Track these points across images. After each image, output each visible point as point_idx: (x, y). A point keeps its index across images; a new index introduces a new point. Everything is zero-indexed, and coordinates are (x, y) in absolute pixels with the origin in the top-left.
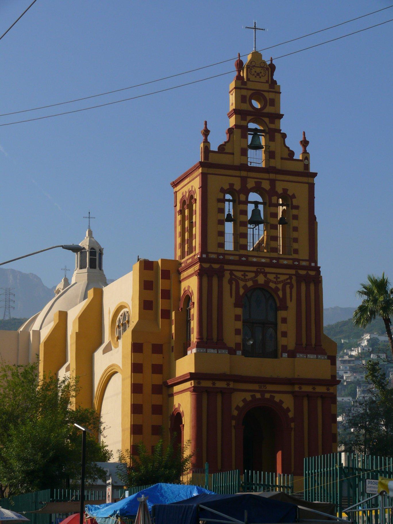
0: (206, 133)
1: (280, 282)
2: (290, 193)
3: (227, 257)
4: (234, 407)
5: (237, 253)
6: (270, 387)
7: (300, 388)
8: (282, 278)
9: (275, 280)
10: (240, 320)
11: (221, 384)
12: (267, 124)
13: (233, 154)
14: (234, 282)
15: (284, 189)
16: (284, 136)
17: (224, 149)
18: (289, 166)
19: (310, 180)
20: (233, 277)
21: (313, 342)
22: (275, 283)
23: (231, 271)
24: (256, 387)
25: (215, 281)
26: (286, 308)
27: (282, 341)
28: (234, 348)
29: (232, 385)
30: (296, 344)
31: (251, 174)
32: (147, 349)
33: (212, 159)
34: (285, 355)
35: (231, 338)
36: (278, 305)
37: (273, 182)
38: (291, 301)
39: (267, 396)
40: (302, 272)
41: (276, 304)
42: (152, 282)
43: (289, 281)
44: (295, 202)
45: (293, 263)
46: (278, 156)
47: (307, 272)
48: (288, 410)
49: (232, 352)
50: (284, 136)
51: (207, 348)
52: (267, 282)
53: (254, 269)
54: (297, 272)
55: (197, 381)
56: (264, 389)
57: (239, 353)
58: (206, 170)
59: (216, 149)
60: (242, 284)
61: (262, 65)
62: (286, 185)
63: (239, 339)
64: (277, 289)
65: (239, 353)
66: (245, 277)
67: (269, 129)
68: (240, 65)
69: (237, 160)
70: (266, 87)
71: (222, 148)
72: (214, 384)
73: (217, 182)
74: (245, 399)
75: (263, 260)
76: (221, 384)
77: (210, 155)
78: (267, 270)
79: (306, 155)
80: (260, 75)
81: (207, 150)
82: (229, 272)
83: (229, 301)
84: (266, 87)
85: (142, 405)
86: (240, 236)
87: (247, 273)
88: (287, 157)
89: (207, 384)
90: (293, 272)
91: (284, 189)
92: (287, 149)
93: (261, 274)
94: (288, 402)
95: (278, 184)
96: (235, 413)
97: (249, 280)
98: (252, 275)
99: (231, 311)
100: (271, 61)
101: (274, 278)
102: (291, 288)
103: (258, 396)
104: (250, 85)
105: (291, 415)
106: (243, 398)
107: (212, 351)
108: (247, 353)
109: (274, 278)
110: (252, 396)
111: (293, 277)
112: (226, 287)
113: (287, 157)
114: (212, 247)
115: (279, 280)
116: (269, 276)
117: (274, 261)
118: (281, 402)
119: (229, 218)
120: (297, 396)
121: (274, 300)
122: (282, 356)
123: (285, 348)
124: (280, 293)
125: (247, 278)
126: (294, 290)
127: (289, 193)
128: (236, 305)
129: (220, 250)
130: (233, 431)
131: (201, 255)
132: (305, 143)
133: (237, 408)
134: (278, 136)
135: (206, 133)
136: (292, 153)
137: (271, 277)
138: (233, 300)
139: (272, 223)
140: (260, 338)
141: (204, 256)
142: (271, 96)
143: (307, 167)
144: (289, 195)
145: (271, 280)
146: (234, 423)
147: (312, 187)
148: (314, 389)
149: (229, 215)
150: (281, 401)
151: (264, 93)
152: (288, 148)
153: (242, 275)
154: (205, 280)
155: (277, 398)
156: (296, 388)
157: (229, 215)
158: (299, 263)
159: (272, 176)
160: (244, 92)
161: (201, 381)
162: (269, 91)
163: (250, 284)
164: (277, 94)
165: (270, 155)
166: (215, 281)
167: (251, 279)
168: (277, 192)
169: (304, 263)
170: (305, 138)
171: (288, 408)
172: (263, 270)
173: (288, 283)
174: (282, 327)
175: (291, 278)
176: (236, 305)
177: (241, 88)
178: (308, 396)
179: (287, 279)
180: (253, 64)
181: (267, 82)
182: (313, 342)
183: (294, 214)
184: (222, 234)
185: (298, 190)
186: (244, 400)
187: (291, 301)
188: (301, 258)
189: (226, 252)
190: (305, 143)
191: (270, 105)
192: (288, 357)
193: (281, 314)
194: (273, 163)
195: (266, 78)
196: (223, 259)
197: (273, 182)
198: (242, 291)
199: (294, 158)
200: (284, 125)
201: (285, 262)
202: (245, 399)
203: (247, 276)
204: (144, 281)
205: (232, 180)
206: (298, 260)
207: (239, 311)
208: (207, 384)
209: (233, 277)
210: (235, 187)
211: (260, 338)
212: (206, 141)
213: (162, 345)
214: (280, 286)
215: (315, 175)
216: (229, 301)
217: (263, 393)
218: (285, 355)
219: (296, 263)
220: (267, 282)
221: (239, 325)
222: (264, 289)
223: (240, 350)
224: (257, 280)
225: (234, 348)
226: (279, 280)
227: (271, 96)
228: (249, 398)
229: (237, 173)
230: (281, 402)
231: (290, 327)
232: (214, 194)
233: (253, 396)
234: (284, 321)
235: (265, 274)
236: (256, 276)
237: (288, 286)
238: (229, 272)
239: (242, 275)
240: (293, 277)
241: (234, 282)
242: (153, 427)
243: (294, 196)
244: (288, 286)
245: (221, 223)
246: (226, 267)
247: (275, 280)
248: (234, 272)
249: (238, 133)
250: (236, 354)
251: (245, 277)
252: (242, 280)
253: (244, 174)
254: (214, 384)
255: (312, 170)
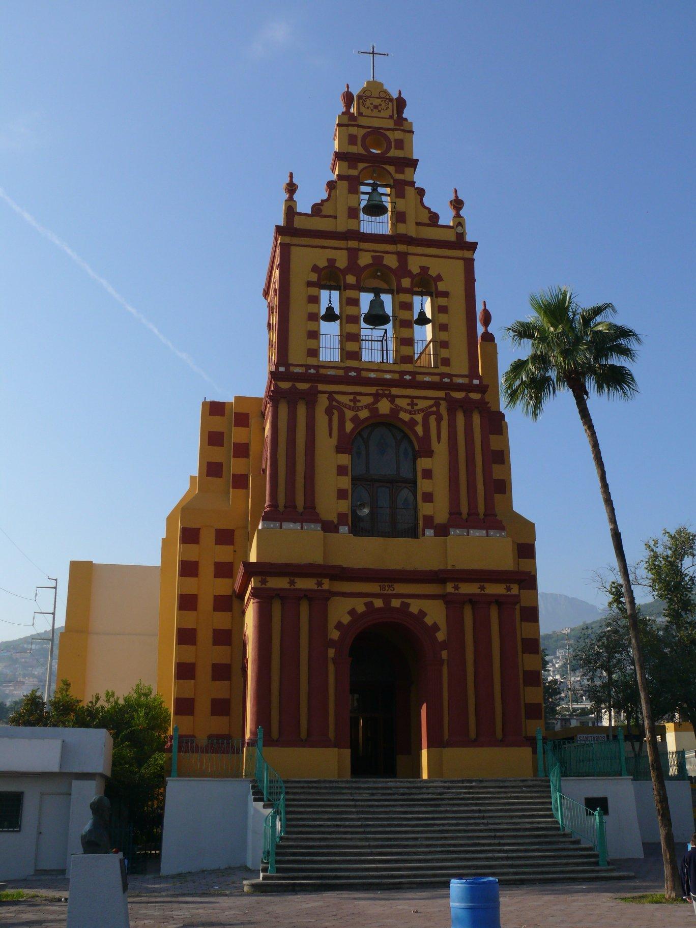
0: (291, 188)
1: (418, 411)
2: (433, 273)
3: (322, 371)
4: (332, 624)
5: (343, 365)
6: (400, 588)
7: (456, 588)
8: (422, 404)
9: (409, 408)
10: (347, 475)
11: (305, 584)
12: (390, 174)
13: (335, 217)
14: (335, 412)
15: (421, 268)
16: (421, 192)
17: (321, 211)
18: (430, 233)
19: (467, 254)
20: (334, 403)
21: (481, 509)
22: (410, 412)
23: (331, 394)
24: (374, 588)
25: (302, 411)
26: (429, 453)
27: (425, 509)
28: (336, 522)
29: (326, 585)
30: (450, 514)
31: (364, 245)
32: (208, 537)
33: (298, 223)
34: (430, 532)
35: (330, 505)
36: (417, 448)
37: (402, 257)
38: (439, 442)
39: (396, 603)
40: (455, 394)
41: (413, 448)
42: (222, 434)
43: (434, 409)
44: (441, 286)
45: (441, 379)
46: (411, 218)
47: (467, 395)
48: (436, 628)
49: (329, 528)
50: (421, 192)
51: (281, 521)
52: (395, 411)
53: (372, 390)
54: (447, 394)
55: (259, 578)
56: (390, 592)
57: (344, 529)
58: (287, 240)
59: (308, 211)
60: (349, 414)
61: (383, 95)
62: (425, 262)
63: (344, 506)
64: (413, 423)
65: (344, 529)
66: (355, 404)
67: (395, 180)
68: (348, 98)
69: (343, 224)
70: (390, 124)
71: (317, 209)
72: (292, 583)
73: (308, 258)
74: (353, 609)
75: (388, 376)
76: (305, 584)
77: (297, 218)
78: (395, 391)
79: (459, 220)
80: (380, 108)
81: (291, 211)
82: (327, 395)
83: (326, 443)
84: (390, 124)
85: (195, 630)
86: (350, 338)
87: (358, 398)
88: (427, 221)
89: (280, 583)
90: (441, 394)
91: (421, 268)
92: (427, 211)
93: (385, 399)
94: (435, 613)
95: (411, 259)
96: (335, 635)
97: (362, 408)
98: (369, 400)
99: (330, 461)
100: (400, 93)
101: (408, 404)
102: (439, 420)
103: (378, 603)
104: (362, 121)
105: (441, 636)
106: (349, 608)
107: (291, 525)
108: (358, 529)
109: (408, 404)
110: (366, 604)
111: (441, 402)
112: (322, 420)
113: (427, 221)
114: (297, 356)
115: (416, 408)
116: (398, 401)
117: (408, 377)
118: (422, 614)
119: (330, 316)
120: (453, 603)
121: (411, 442)
122: (424, 535)
123: (429, 521)
124: (419, 429)
125: (358, 404)
126: (444, 424)
127: (430, 272)
128: (339, 449)
129: (311, 361)
130: (331, 668)
131: (277, 368)
132: (457, 204)
133: (339, 626)
134: (409, 191)
135: (291, 188)
136: (434, 217)
137: (403, 403)
138: (334, 441)
139: (403, 318)
140: (383, 504)
141: (282, 369)
142: (398, 135)
143: (461, 236)
144: (431, 276)
145: (402, 408)
146: (331, 652)
147: (469, 265)
148: (482, 588)
149: (330, 309)
150: (421, 611)
151: (388, 133)
152: (429, 209)
153: (351, 401)
154: (283, 410)
155: (415, 607)
156: (450, 588)
157: (330, 309)
158: (451, 380)
159: (402, 248)
160: (353, 130)
161: (268, 579)
162: (393, 130)
163: (364, 414)
164: (407, 134)
165: (399, 217)
166: (302, 411)
167: (367, 407)
168: (410, 272)
169: (460, 381)
170: (457, 197)
171: (435, 624)
172: (387, 392)
173: (433, 413)
174: (424, 486)
175: (437, 405)
176: (339, 449)
177: (347, 126)
178: (472, 600)
179: (431, 407)
180: (368, 93)
181: (391, 117)
182: (481, 509)
183: (440, 303)
184: (314, 335)
185: (447, 269)
186: (352, 612)
187: (439, 442)
188: (454, 373)
189: (322, 364)
190: (457, 204)
191: (396, 148)
192: (435, 535)
193: (423, 463)
194: (402, 229)
195: (389, 112)
196: (318, 375)
197: (402, 257)
198: (349, 426)
199: (440, 223)
200: (420, 178)
201: (427, 379)
202: (353, 609)
203: (359, 401)
204: (210, 432)
205: (331, 254)
206: (450, 376)
207: (345, 459)
208: (280, 583)
209: (334, 403)
210: (337, 265)
211: (383, 504)
212: (291, 199)
213: (233, 531)
214: (419, 418)
215: (473, 246)
216: (326, 443)
217: (387, 598)
218: (430, 532)
219: (447, 380)
220: (395, 411)
221: (345, 482)
222: (390, 424)
223: (346, 524)
224: (377, 409)
225: (336, 522)
226: (416, 408)
227: (398, 135)
228: (361, 609)
229: (342, 244)
230: (422, 614)
231: (439, 485)
232: (301, 272)
233: (369, 605)
234: (428, 474)
235: (392, 398)
236: (376, 401)
237: (432, 419)
238: (327, 395)
239: (351, 401)
240: (441, 402)
241: (335, 412)
242: (214, 666)
243: (439, 278)
244: (432, 419)
245: (314, 317)
246: (321, 387)
247: (409, 408)
248: (337, 397)
249: (343, 186)
250: (338, 532)
251: (355, 404)
252: (349, 408)
253: (353, 244)
254: (292, 583)
255: (469, 238)
